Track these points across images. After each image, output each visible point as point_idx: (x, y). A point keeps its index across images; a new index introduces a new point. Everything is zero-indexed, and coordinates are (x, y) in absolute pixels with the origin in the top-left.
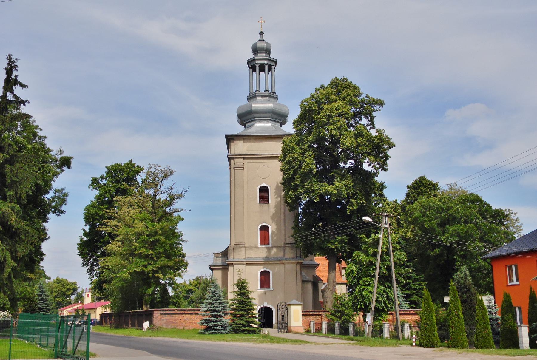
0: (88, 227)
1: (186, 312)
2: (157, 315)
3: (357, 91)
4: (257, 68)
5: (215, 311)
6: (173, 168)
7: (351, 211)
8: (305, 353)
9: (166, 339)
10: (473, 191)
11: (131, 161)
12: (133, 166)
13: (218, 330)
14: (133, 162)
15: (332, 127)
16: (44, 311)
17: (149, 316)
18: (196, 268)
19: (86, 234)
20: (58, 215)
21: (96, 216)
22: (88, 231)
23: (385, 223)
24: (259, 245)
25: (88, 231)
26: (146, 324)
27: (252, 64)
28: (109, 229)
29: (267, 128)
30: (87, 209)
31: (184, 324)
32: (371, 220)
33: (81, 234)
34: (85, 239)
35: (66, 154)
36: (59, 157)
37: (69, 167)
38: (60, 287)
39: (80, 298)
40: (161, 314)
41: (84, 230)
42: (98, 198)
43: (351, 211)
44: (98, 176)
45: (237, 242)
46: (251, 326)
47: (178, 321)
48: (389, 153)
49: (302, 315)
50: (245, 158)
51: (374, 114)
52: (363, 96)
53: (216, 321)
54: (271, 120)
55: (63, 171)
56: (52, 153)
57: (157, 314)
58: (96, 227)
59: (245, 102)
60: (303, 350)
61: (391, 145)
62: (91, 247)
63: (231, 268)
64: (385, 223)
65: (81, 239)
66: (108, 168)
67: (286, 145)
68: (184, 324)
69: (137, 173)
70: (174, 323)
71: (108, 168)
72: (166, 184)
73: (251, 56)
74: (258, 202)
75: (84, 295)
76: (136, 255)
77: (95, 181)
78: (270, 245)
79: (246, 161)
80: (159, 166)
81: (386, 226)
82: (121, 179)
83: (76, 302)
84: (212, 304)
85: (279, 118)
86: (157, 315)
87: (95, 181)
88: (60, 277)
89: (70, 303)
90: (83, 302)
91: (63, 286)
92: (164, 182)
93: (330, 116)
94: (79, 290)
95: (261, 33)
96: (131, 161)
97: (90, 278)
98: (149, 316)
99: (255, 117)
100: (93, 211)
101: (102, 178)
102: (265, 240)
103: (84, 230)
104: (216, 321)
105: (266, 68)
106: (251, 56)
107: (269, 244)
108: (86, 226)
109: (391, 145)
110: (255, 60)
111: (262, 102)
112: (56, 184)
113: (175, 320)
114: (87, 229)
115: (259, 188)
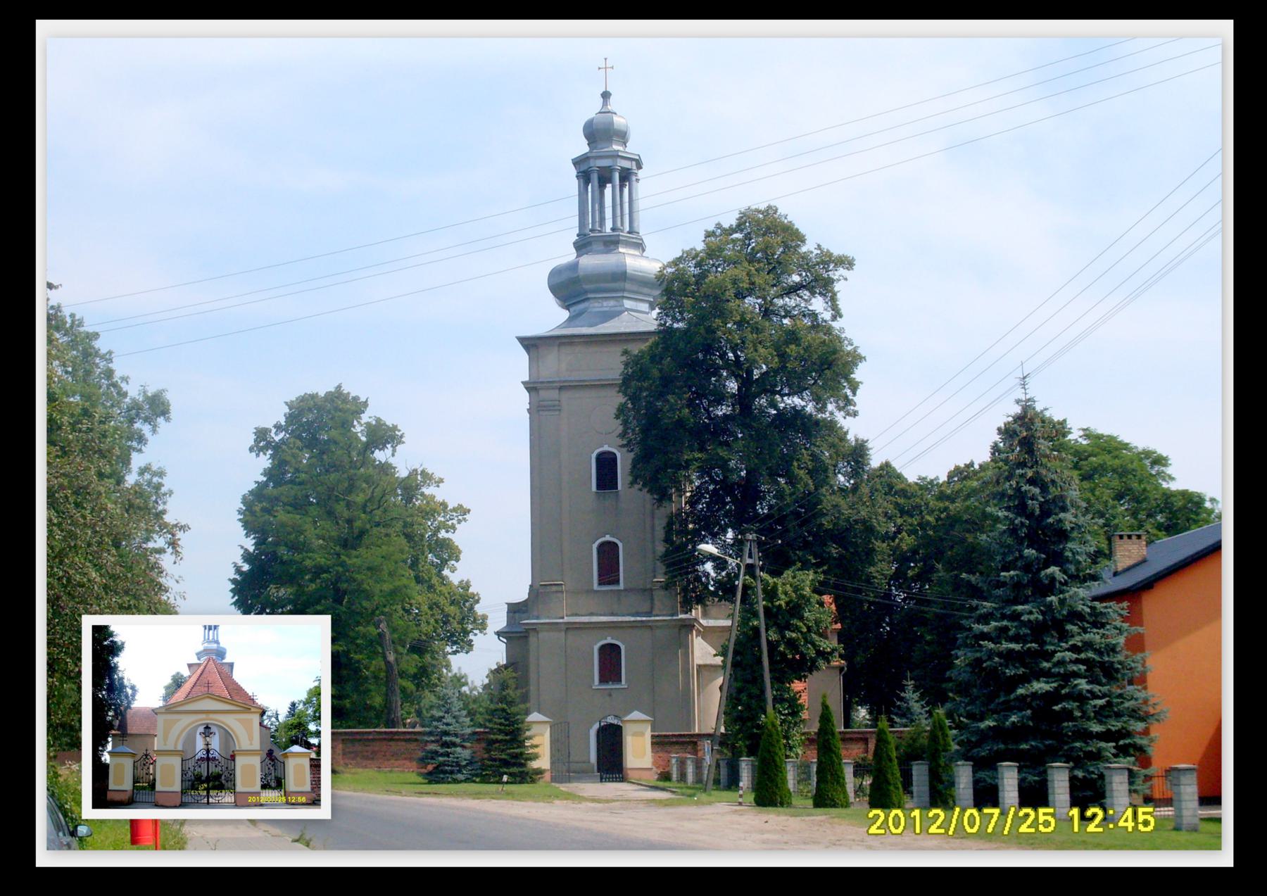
4: (595, 177)
5: (446, 733)
8: (516, 818)
9: (372, 796)
19: (247, 557)
22: (251, 549)
24: (596, 587)
25: (251, 549)
27: (584, 168)
34: (246, 567)
42: (268, 473)
44: (269, 424)
50: (561, 388)
59: (569, 255)
60: (500, 811)
63: (533, 639)
65: (238, 570)
73: (583, 148)
74: (594, 488)
76: (816, 489)
77: (261, 434)
78: (621, 586)
79: (565, 396)
81: (749, 561)
85: (646, 290)
87: (261, 434)
95: (606, 95)
96: (339, 387)
99: (586, 292)
101: (278, 427)
102: (608, 571)
105: (617, 176)
106: (583, 148)
107: (617, 582)
114: (250, 544)
115: (594, 456)
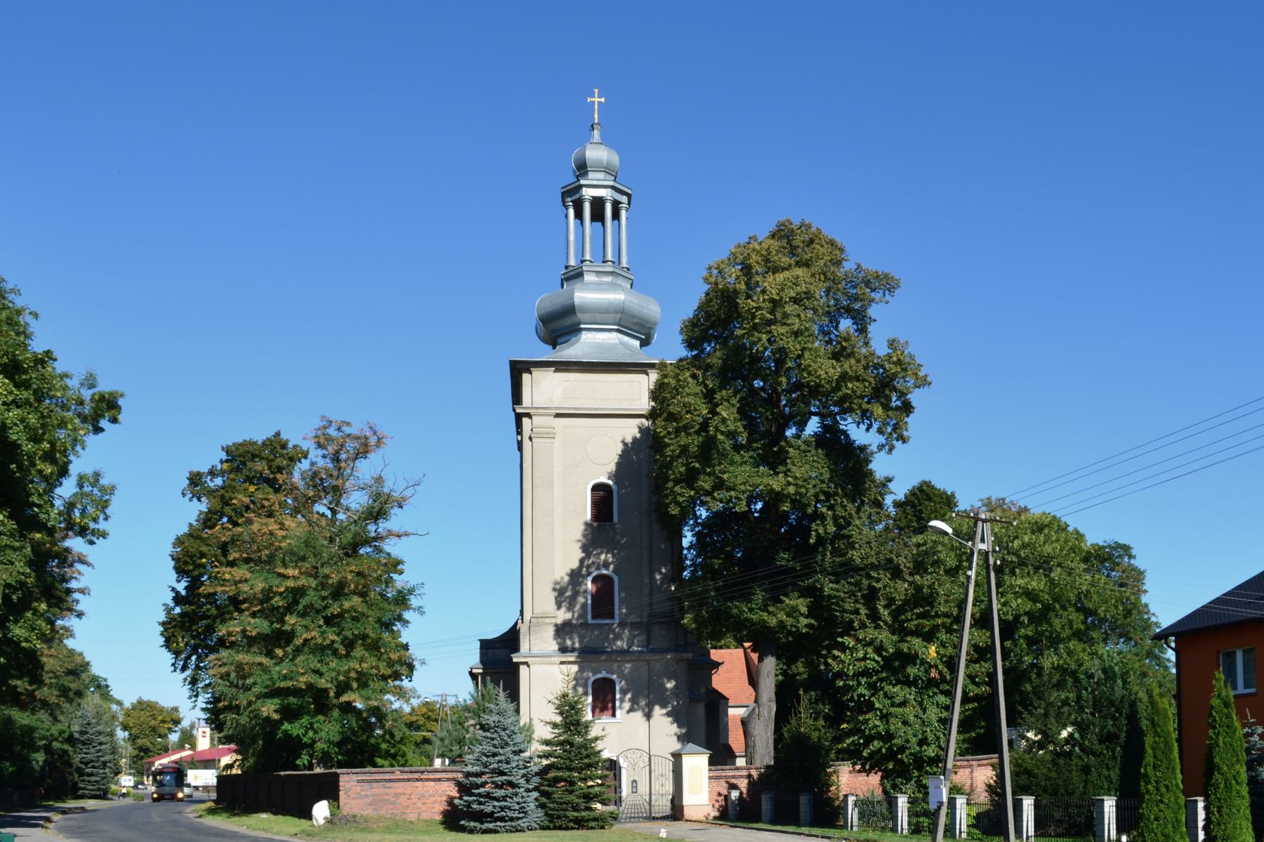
0: (184, 584)
1: (423, 776)
2: (348, 785)
3: (836, 253)
6: (383, 429)
7: (818, 535)
10: (1048, 509)
11: (278, 434)
12: (284, 446)
13: (512, 819)
14: (284, 436)
15: (783, 330)
16: (93, 767)
17: (330, 790)
18: (440, 673)
19: (178, 599)
20: (92, 543)
21: (201, 558)
22: (183, 593)
23: (983, 540)
25: (183, 593)
26: (321, 810)
28: (231, 590)
29: (610, 348)
30: (179, 541)
31: (419, 804)
32: (950, 530)
33: (168, 598)
34: (178, 610)
35: (104, 386)
36: (87, 394)
37: (114, 420)
38: (144, 716)
39: (188, 738)
40: (359, 781)
41: (173, 589)
43: (818, 535)
45: (538, 611)
46: (589, 809)
47: (403, 799)
48: (915, 397)
49: (710, 778)
50: (558, 415)
51: (872, 312)
52: (848, 266)
53: (504, 798)
54: (618, 331)
55: (102, 430)
56: (69, 382)
57: (349, 781)
58: (202, 583)
61: (923, 382)
62: (192, 628)
64: (983, 540)
65: (169, 610)
66: (228, 450)
67: (665, 376)
68: (419, 804)
69: (292, 460)
70: (393, 803)
71: (228, 450)
72: (365, 470)
75: (194, 732)
77: (195, 480)
80: (348, 424)
81: (983, 547)
82: (254, 469)
83: (180, 747)
84: (494, 755)
86: (348, 785)
87: (195, 480)
88: (145, 698)
89: (166, 750)
90: (193, 747)
91: (154, 717)
92: (362, 464)
93: (776, 304)
94: (185, 724)
96: (278, 434)
97: (190, 697)
98: (330, 790)
100: (194, 546)
101: (212, 473)
103: (173, 589)
104: (504, 798)
105: (609, 207)
108: (178, 581)
109: (923, 382)
110: (581, 186)
111: (599, 287)
112: (80, 465)
113: (397, 795)
114: (181, 587)
